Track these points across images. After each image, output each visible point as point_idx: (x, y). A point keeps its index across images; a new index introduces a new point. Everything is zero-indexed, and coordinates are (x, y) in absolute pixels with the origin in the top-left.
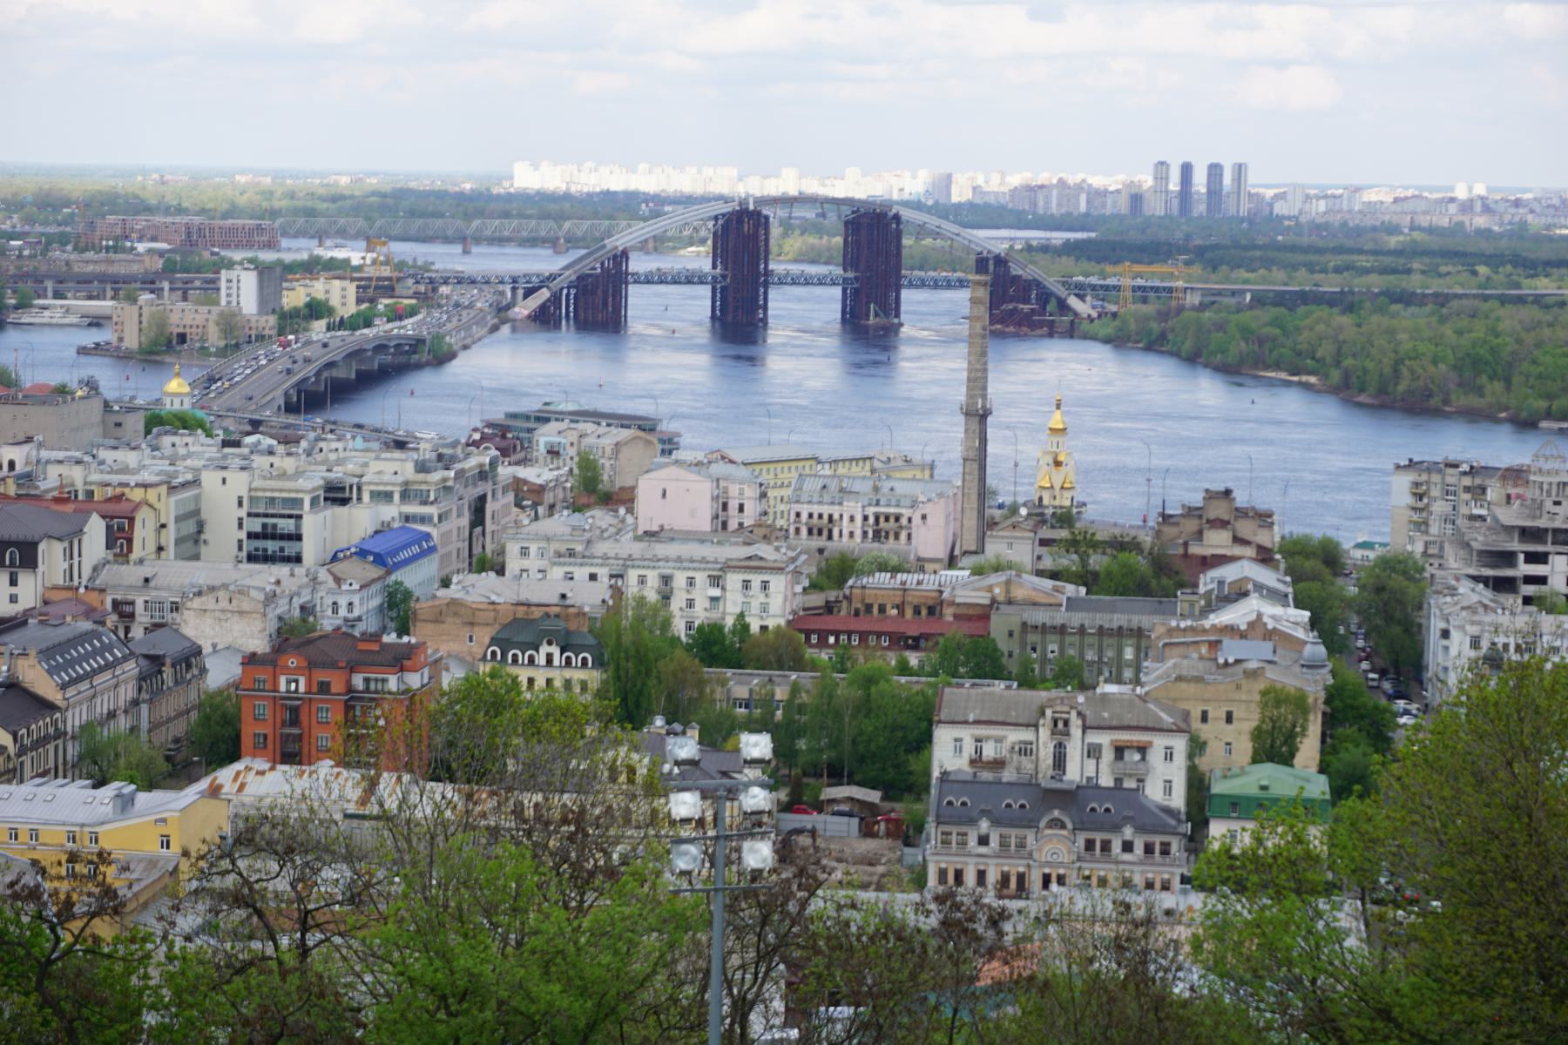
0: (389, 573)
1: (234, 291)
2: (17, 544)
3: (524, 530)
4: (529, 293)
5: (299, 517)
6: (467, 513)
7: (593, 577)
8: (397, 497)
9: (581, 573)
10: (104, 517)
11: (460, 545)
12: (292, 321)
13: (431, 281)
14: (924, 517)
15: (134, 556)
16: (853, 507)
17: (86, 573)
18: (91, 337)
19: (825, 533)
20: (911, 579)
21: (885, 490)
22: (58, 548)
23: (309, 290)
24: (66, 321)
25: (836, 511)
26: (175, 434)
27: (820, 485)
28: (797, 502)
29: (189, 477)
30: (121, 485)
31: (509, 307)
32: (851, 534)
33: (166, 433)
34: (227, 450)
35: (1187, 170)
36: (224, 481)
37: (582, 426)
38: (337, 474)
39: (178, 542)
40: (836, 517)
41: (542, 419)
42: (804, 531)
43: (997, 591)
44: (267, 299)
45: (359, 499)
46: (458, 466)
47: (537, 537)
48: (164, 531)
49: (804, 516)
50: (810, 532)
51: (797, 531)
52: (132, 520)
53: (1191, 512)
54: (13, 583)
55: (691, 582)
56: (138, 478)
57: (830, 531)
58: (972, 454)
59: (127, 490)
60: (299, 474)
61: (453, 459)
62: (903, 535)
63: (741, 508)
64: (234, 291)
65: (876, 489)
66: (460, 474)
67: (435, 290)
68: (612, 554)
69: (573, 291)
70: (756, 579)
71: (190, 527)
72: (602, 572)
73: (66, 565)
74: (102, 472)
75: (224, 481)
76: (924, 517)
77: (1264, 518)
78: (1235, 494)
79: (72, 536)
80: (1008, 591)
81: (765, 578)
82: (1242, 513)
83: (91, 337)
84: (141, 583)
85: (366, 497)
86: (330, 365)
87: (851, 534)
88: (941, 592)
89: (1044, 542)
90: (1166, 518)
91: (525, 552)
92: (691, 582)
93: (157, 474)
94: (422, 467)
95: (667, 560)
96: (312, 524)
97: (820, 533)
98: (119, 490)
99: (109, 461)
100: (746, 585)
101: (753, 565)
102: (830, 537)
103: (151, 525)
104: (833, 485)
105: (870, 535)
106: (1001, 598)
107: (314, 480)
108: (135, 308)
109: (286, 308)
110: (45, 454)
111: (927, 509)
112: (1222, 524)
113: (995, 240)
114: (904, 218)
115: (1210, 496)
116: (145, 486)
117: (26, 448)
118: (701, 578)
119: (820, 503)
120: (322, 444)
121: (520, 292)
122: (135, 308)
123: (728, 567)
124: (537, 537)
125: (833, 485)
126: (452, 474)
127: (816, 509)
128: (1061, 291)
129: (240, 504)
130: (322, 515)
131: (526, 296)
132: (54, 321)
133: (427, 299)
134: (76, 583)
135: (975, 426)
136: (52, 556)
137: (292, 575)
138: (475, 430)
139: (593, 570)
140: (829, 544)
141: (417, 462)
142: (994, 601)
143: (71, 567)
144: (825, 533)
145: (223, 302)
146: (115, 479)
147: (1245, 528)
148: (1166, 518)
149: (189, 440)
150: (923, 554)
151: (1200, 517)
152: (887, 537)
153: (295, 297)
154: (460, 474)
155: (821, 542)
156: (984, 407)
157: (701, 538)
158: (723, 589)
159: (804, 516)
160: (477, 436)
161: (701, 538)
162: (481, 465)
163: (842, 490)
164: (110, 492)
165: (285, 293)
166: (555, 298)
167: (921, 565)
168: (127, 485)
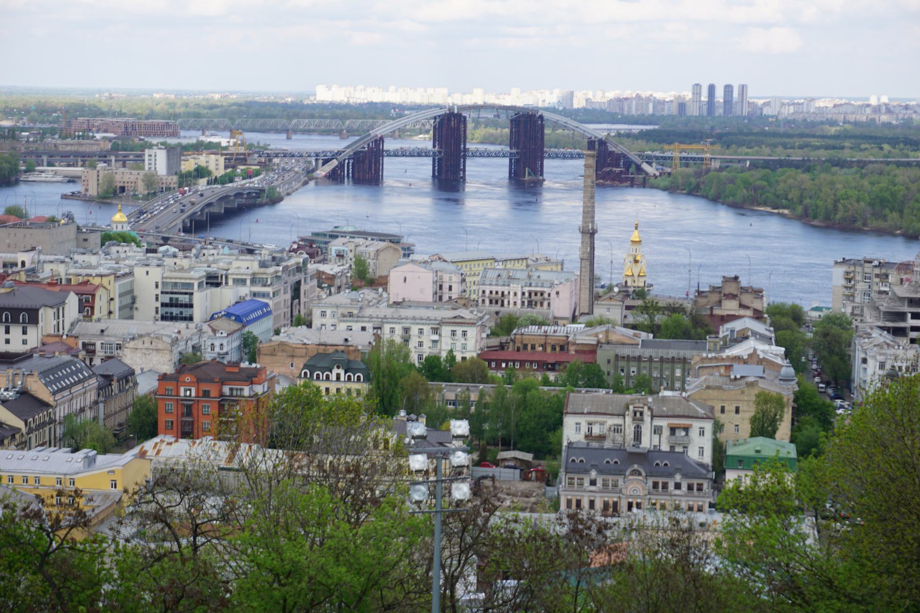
0: (244, 326)
3: (323, 301)
4: (325, 162)
5: (192, 294)
6: (289, 291)
7: (363, 329)
8: (248, 282)
9: (357, 326)
10: (77, 294)
11: (285, 310)
12: (187, 179)
13: (268, 155)
14: (558, 293)
15: (95, 317)
16: (516, 287)
17: (67, 327)
18: (69, 189)
19: (500, 302)
20: (550, 329)
21: (535, 277)
22: (51, 312)
24: (55, 179)
26: (119, 245)
28: (483, 284)
29: (127, 270)
30: (87, 275)
32: (515, 303)
33: (113, 245)
34: (150, 255)
35: (712, 88)
36: (147, 273)
37: (356, 240)
38: (214, 268)
39: (121, 309)
40: (506, 293)
41: (334, 236)
42: (487, 301)
43: (601, 336)
45: (227, 283)
46: (284, 264)
47: (331, 306)
48: (112, 302)
49: (487, 293)
50: (491, 302)
51: (483, 301)
52: (93, 296)
53: (715, 290)
54: (25, 332)
55: (421, 331)
57: (503, 302)
58: (586, 256)
59: (90, 279)
60: (191, 268)
61: (282, 260)
62: (545, 304)
63: (450, 288)
65: (530, 277)
66: (285, 268)
67: (270, 160)
68: (375, 315)
69: (351, 161)
70: (459, 330)
71: (127, 300)
72: (369, 326)
73: (55, 322)
74: (76, 268)
75: (147, 273)
76: (558, 293)
77: (758, 293)
78: (740, 279)
79: (58, 306)
80: (607, 336)
82: (745, 290)
83: (69, 189)
84: (99, 332)
85: (230, 282)
87: (515, 303)
88: (568, 337)
90: (700, 293)
91: (323, 314)
92: (421, 331)
93: (108, 269)
94: (263, 265)
95: (407, 319)
97: (497, 302)
98: (86, 278)
99: (80, 261)
100: (454, 333)
101: (457, 321)
102: (502, 305)
103: (105, 299)
104: (504, 274)
105: (526, 303)
106: (603, 341)
107: (200, 272)
108: (95, 172)
109: (183, 171)
110: (42, 257)
111: (559, 288)
112: (733, 297)
113: (599, 130)
114: (545, 118)
115: (726, 280)
116: (101, 276)
117: (32, 254)
118: (427, 329)
119: (497, 285)
120: (205, 251)
121: (320, 162)
122: (95, 172)
123: (443, 322)
124: (331, 306)
125: (504, 274)
126: (281, 268)
127: (494, 289)
128: (638, 160)
129: (157, 286)
130: (205, 292)
131: (323, 164)
132: (48, 179)
134: (61, 333)
135: (588, 240)
136: (47, 317)
137: (187, 328)
138: (294, 243)
139: (364, 325)
140: (502, 309)
141: (260, 261)
142: (599, 342)
143: (58, 323)
144: (500, 302)
145: (147, 168)
146: (84, 272)
147: (747, 299)
148: (700, 293)
149: (127, 249)
150: (557, 315)
151: (720, 292)
152: (536, 305)
153: (188, 165)
154: (285, 268)
155: (497, 308)
156: (593, 228)
157: (427, 306)
158: (440, 335)
159: (487, 293)
160: (295, 246)
161: (427, 306)
163: (509, 277)
164: (81, 279)
165: (183, 163)
166: (341, 165)
167: (556, 321)
168: (91, 275)
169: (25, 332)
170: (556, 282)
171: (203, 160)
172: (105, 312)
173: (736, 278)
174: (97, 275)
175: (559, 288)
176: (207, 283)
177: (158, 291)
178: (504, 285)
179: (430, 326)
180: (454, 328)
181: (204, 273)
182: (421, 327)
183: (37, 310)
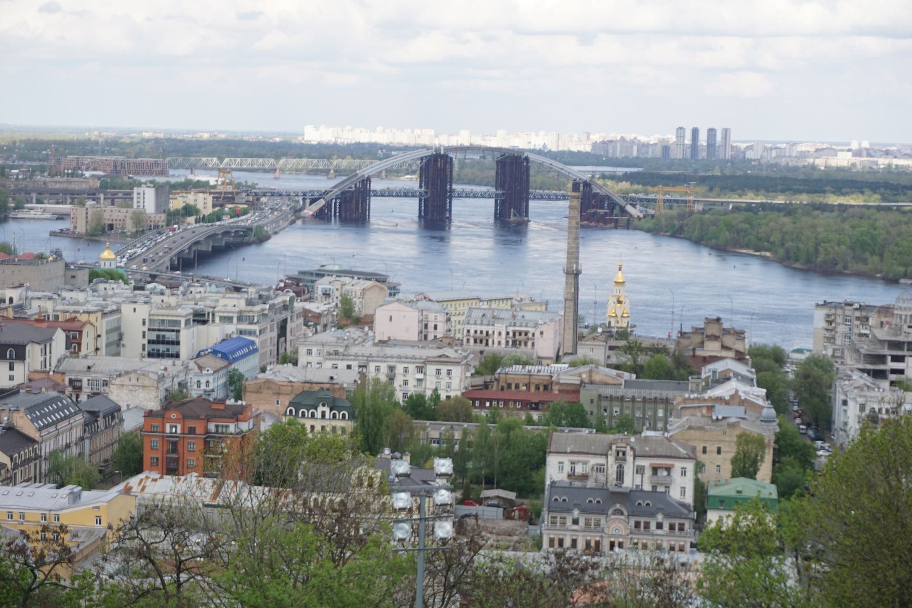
0: (230, 364)
1: (141, 200)
2: (13, 346)
3: (309, 339)
4: (313, 201)
5: (178, 331)
6: (276, 329)
7: (349, 367)
8: (235, 320)
9: (342, 365)
10: (64, 331)
11: (272, 348)
12: (175, 217)
13: (256, 194)
14: (542, 333)
16: (500, 327)
17: (54, 363)
18: (58, 226)
19: (484, 342)
20: (534, 369)
22: (38, 348)
23: (185, 199)
25: (490, 329)
27: (481, 314)
29: (114, 307)
30: (75, 312)
31: (301, 209)
32: (499, 343)
35: (695, 132)
36: (135, 310)
37: (343, 279)
38: (201, 306)
39: (108, 345)
40: (490, 332)
41: (320, 275)
42: (472, 341)
43: (584, 376)
44: (161, 205)
45: (213, 321)
46: (271, 302)
47: (316, 344)
48: (99, 339)
49: (472, 332)
50: (475, 341)
51: (468, 340)
52: (81, 332)
53: (697, 331)
54: (11, 368)
55: (406, 370)
56: (85, 308)
57: (487, 341)
58: (570, 297)
59: (78, 315)
62: (530, 343)
64: (141, 200)
65: (514, 317)
66: (272, 307)
67: (258, 199)
69: (338, 201)
70: (444, 369)
72: (355, 364)
74: (63, 304)
75: (135, 310)
76: (542, 333)
78: (722, 321)
79: (45, 342)
80: (590, 376)
81: (449, 368)
82: (727, 332)
83: (58, 226)
84: (85, 369)
85: (217, 320)
86: (197, 243)
87: (499, 343)
88: (551, 377)
89: (611, 348)
90: (682, 334)
91: (309, 352)
92: (406, 370)
94: (250, 303)
95: (392, 357)
96: (185, 335)
97: (481, 342)
98: (73, 315)
99: (68, 298)
100: (438, 372)
102: (487, 344)
103: (92, 335)
104: (489, 314)
105: (510, 343)
106: (586, 381)
107: (187, 310)
108: (85, 209)
109: (172, 209)
111: (544, 328)
112: (715, 338)
114: (531, 159)
115: (709, 321)
116: (89, 313)
118: (412, 367)
120: (192, 289)
121: (308, 201)
122: (84, 210)
123: (427, 361)
124: (316, 344)
125: (489, 314)
126: (267, 306)
127: (479, 328)
129: (144, 323)
130: (191, 330)
131: (311, 204)
132: (37, 216)
133: (254, 205)
135: (572, 280)
136: (34, 353)
138: (281, 281)
139: (349, 363)
140: (487, 348)
142: (582, 382)
144: (484, 342)
145: (135, 206)
146: (71, 308)
148: (682, 334)
149: (115, 286)
151: (703, 334)
152: (520, 344)
153: (177, 203)
154: (272, 307)
155: (481, 347)
156: (577, 269)
157: (412, 345)
158: (425, 374)
159: (472, 332)
160: (282, 285)
161: (412, 345)
162: (284, 302)
163: (494, 317)
164: (68, 316)
166: (328, 205)
167: (540, 361)
168: (78, 312)
169: (11, 368)
170: (541, 322)
171: (191, 198)
172: (92, 348)
173: (718, 320)
174: (84, 312)
175: (544, 328)
176: (194, 321)
177: (146, 328)
178: (488, 325)
179: (415, 365)
180: (439, 367)
181: (191, 311)
182: (406, 365)
183: (23, 347)
